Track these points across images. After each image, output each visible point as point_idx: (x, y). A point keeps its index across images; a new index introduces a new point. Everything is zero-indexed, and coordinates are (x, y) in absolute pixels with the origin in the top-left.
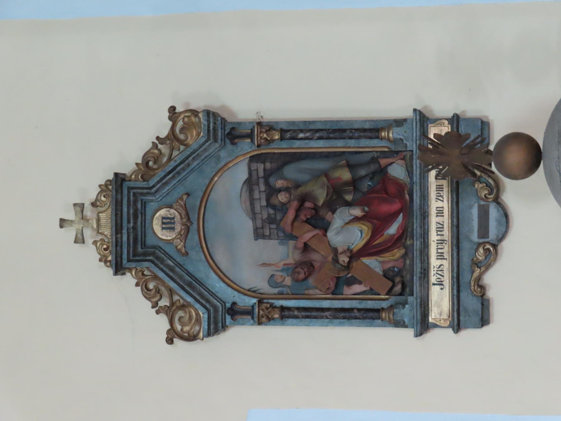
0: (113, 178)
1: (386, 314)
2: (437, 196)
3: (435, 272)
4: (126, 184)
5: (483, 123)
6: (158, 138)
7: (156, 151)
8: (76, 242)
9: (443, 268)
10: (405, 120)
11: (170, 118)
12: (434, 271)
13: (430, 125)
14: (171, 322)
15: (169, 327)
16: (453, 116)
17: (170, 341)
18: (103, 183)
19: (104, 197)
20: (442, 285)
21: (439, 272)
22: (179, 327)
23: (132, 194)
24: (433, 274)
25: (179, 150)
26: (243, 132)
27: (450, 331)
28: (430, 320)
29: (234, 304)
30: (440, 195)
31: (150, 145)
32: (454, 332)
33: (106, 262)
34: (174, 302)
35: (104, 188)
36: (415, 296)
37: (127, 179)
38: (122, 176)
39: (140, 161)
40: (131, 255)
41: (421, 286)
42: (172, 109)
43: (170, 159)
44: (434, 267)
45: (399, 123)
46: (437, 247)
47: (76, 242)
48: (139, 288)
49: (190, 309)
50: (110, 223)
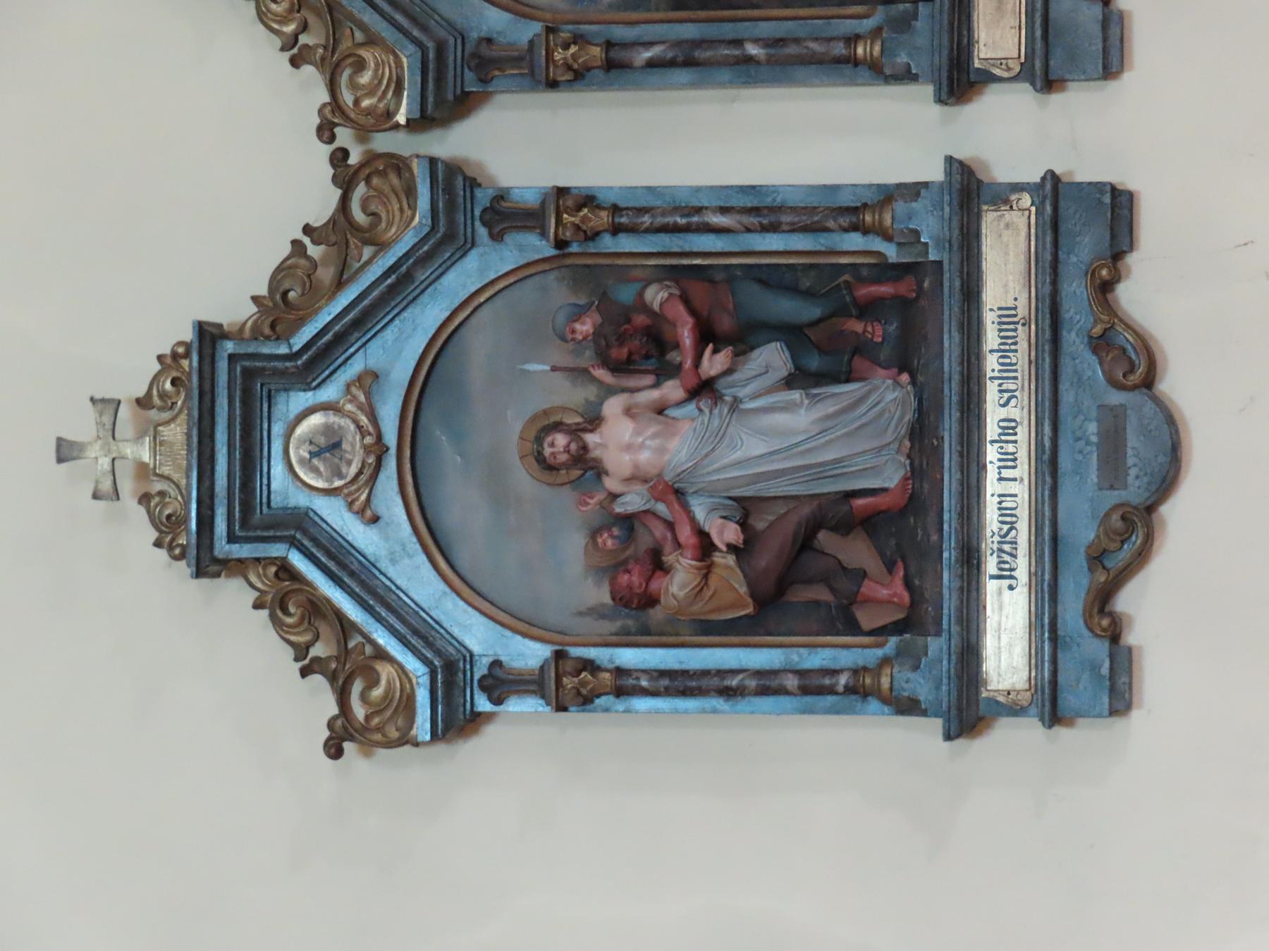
1: (871, 54)
2: (1002, 338)
3: (995, 546)
5: (1115, 191)
7: (302, 262)
9: (1014, 538)
10: (926, 185)
16: (1044, 179)
17: (334, 750)
18: (167, 351)
19: (173, 383)
20: (1011, 577)
21: (1007, 547)
22: (347, 98)
29: (496, 664)
30: (1008, 361)
31: (287, 249)
33: (171, 548)
39: (263, 290)
40: (247, 364)
42: (340, 155)
44: (994, 534)
45: (914, 190)
48: (264, 613)
50: (185, 456)
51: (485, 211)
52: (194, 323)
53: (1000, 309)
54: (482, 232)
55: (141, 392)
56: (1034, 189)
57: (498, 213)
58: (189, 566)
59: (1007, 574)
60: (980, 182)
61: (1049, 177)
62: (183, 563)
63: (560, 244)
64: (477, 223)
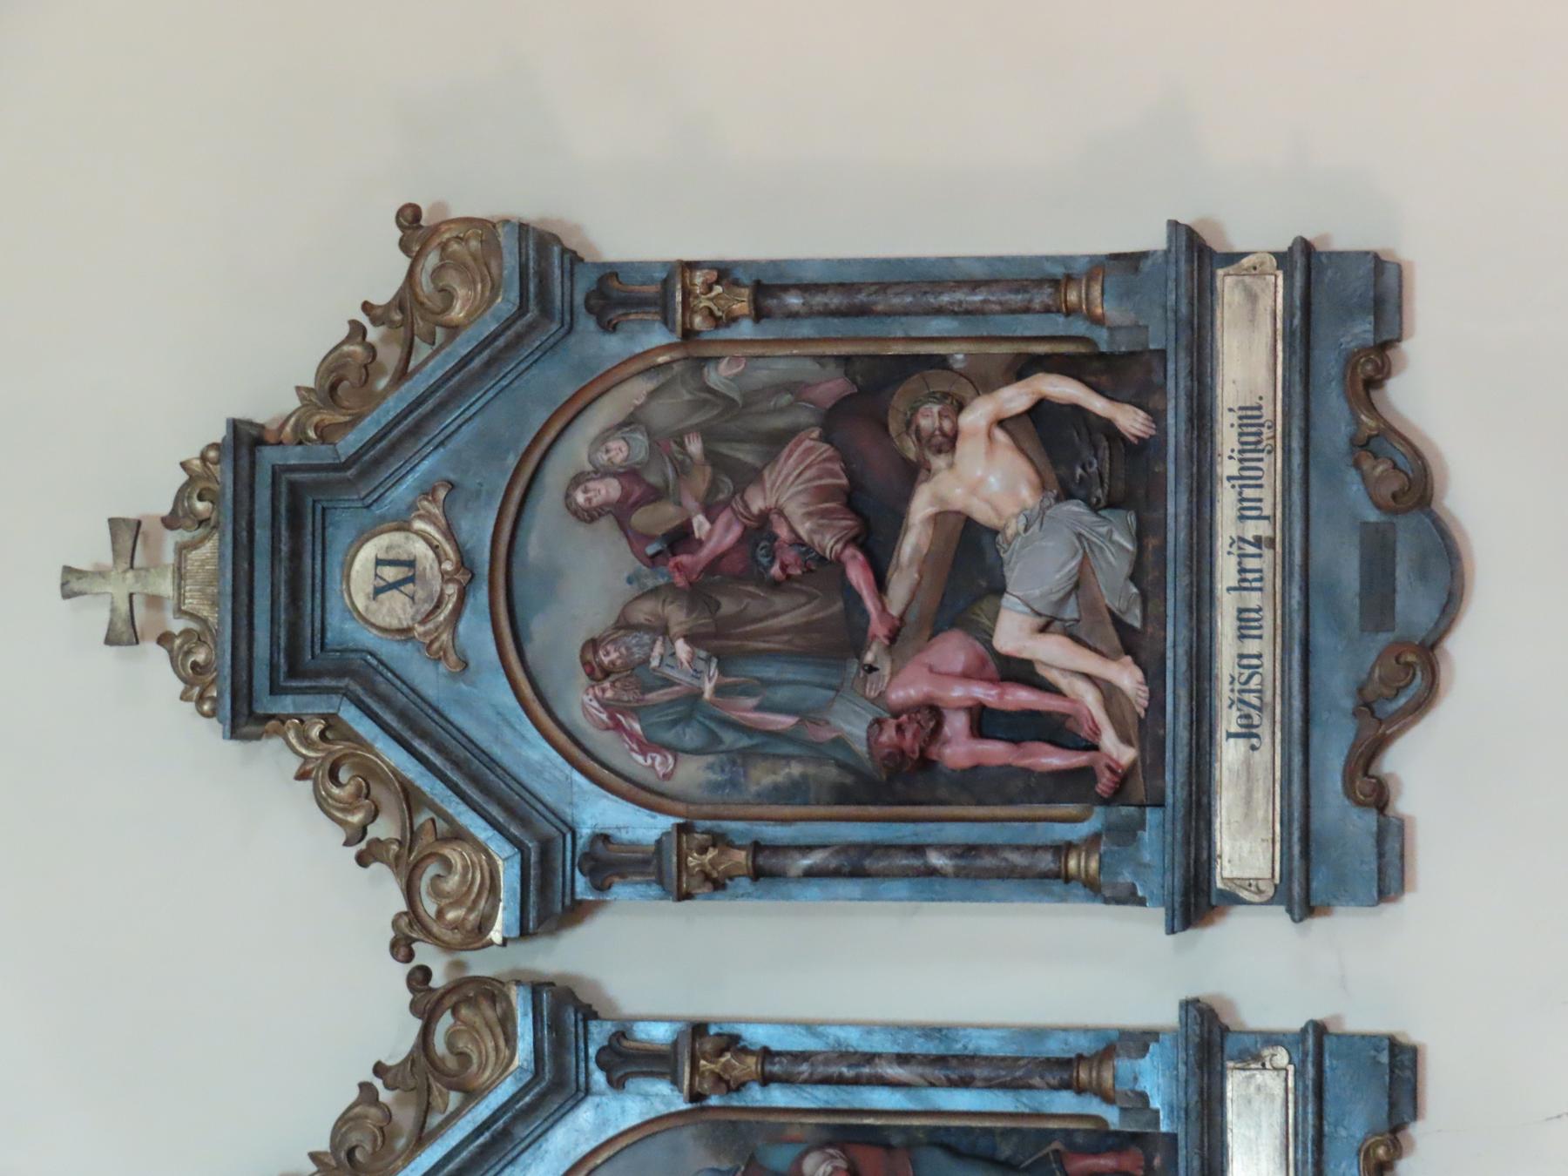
0: (224, 439)
1: (1087, 871)
4: (269, 456)
6: (367, 307)
8: (109, 641)
11: (404, 246)
12: (1232, 691)
13: (1220, 272)
14: (410, 893)
15: (402, 906)
22: (429, 906)
23: (284, 488)
24: (1230, 541)
25: (433, 343)
26: (632, 291)
27: (1279, 915)
28: (1219, 885)
31: (354, 1094)
32: (1294, 920)
33: (201, 699)
34: (415, 828)
35: (196, 482)
36: (1169, 810)
37: (270, 438)
38: (254, 432)
39: (310, 383)
41: (1193, 252)
42: (409, 212)
43: (402, 374)
45: (1139, 1041)
46: (1240, 505)
47: (109, 641)
49: (445, 629)
51: (601, 1051)
52: (228, 421)
53: (1241, 408)
54: (599, 1077)
55: (166, 509)
56: (1283, 259)
57: (619, 1054)
58: (220, 722)
59: (1249, 417)
60: (1225, 1030)
61: (1298, 249)
62: (214, 721)
63: (695, 1097)
64: (593, 1065)
